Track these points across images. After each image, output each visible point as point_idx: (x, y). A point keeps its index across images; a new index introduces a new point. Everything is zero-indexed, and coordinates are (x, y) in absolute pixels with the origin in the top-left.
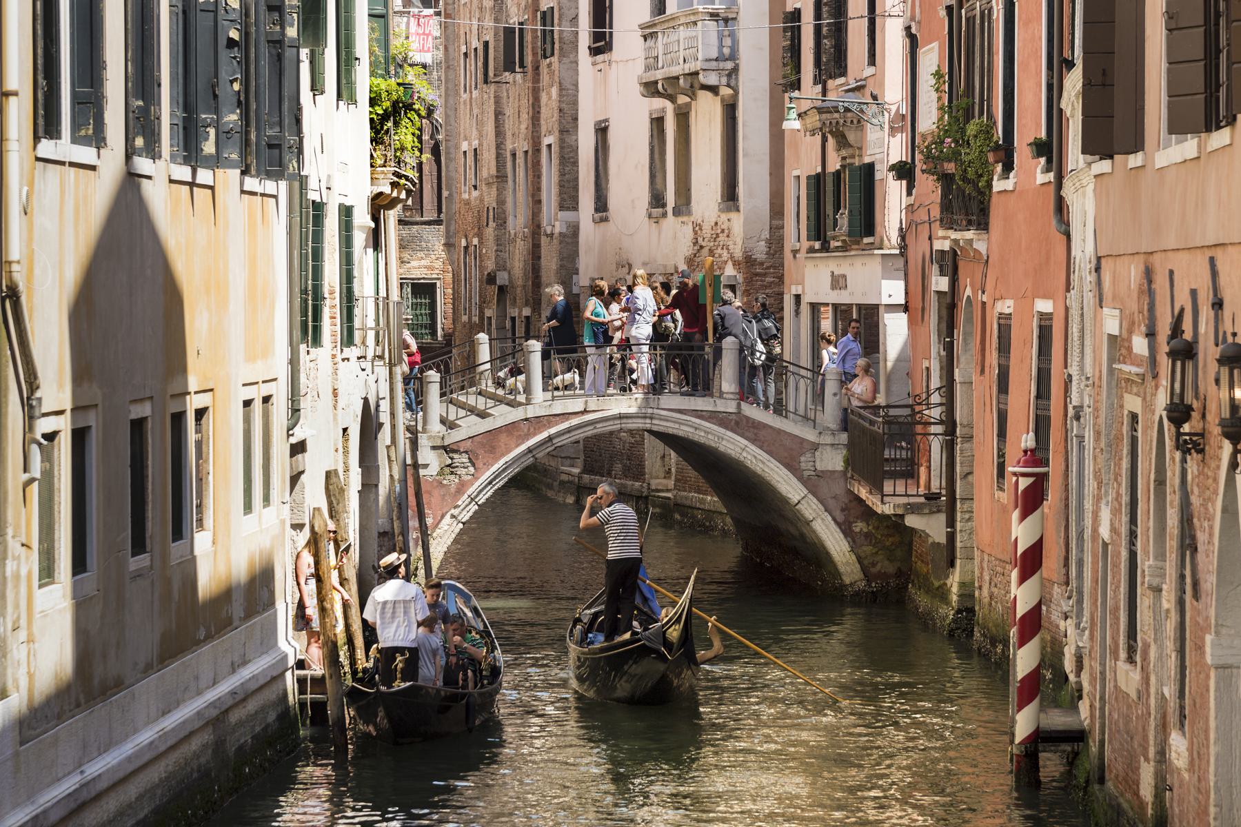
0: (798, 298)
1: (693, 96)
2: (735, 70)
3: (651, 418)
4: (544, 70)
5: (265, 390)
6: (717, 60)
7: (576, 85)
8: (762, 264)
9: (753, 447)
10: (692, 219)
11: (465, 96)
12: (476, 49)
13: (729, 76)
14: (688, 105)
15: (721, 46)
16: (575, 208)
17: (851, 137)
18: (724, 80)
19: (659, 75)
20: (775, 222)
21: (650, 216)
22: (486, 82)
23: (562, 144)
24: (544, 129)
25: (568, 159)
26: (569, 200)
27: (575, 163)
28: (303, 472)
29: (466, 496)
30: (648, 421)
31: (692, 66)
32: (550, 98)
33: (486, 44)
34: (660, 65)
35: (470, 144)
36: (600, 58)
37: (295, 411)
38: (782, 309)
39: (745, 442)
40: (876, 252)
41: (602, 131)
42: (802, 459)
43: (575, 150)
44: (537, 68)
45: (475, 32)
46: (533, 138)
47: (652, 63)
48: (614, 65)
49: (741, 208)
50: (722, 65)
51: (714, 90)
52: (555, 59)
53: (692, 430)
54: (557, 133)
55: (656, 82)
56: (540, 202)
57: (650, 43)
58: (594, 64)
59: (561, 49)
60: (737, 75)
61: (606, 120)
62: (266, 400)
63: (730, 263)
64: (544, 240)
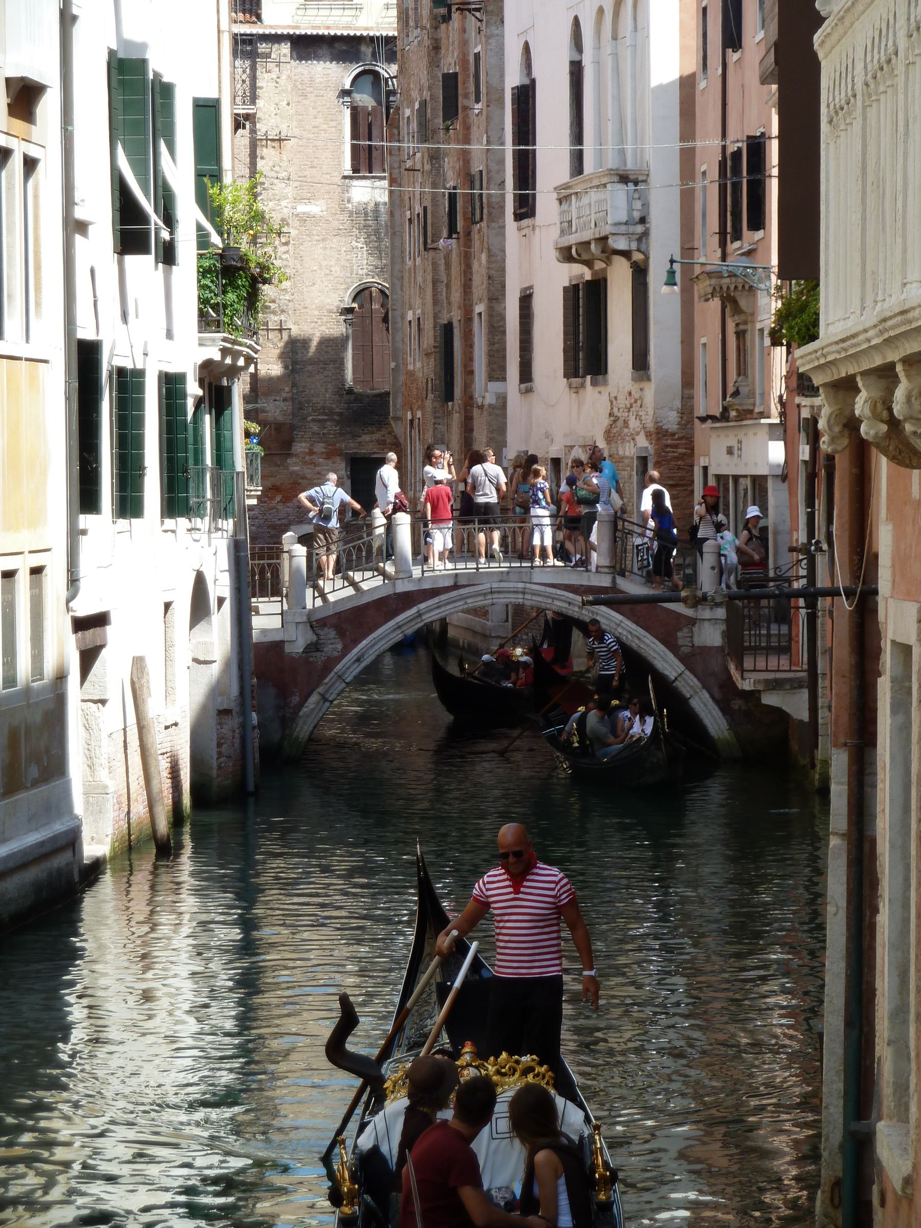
0: (705, 469)
1: (608, 261)
2: (646, 234)
3: (524, 593)
4: (475, 236)
5: (36, 561)
6: (626, 223)
7: (504, 251)
8: (673, 434)
9: (629, 623)
10: (609, 389)
11: (409, 263)
12: (418, 215)
13: (639, 240)
14: (604, 271)
15: (630, 210)
16: (504, 379)
17: (743, 303)
18: (634, 246)
19: (572, 239)
20: (687, 392)
21: (570, 387)
22: (426, 249)
23: (491, 311)
24: (475, 297)
25: (497, 329)
26: (497, 372)
27: (504, 333)
28: (102, 647)
29: (332, 674)
30: (520, 596)
31: (606, 230)
32: (480, 264)
33: (425, 209)
34: (574, 229)
35: (414, 314)
36: (525, 222)
37: (73, 581)
38: (693, 482)
39: (620, 617)
40: (763, 421)
41: (526, 300)
42: (679, 634)
43: (503, 318)
44: (468, 234)
45: (417, 197)
46: (465, 306)
47: (567, 227)
48: (537, 229)
49: (653, 377)
50: (631, 229)
51: (626, 254)
52: (484, 224)
53: (566, 605)
54: (486, 301)
55: (570, 248)
56: (472, 372)
57: (565, 206)
58: (519, 229)
59: (490, 214)
60: (647, 239)
61: (531, 287)
62: (36, 571)
63: (642, 434)
64: (476, 412)
